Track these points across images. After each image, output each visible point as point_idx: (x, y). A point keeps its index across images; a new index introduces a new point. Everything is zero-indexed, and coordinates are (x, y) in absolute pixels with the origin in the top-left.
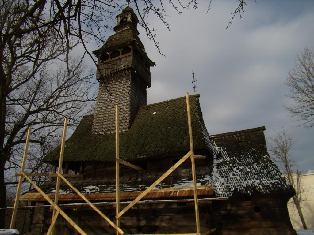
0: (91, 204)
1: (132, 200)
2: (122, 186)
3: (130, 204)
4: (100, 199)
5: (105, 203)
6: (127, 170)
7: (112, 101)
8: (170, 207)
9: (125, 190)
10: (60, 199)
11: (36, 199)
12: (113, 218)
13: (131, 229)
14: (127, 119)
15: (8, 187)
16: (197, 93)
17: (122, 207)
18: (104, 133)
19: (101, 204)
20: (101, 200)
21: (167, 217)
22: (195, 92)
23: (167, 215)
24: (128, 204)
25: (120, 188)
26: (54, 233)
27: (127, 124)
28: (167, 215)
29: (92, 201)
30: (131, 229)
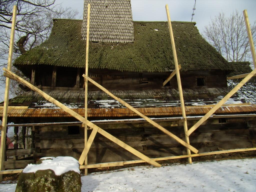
0: (149, 120)
1: (204, 114)
2: (153, 101)
3: (202, 118)
4: (156, 114)
5: (105, 121)
6: (147, 84)
7: (107, 7)
8: (212, 124)
9: (161, 105)
10: (8, 114)
11: (24, 114)
12: (183, 137)
13: (172, 149)
14: (131, 29)
15: (113, 90)
16: (193, 21)
17: (191, 123)
18: (100, 41)
19: (115, 122)
20: (167, 115)
21: (209, 134)
22: (192, 19)
23: (209, 131)
24: (197, 120)
25: (180, 104)
26: (255, 147)
27: (131, 35)
28: (209, 131)
29: (149, 117)
30: (172, 149)
